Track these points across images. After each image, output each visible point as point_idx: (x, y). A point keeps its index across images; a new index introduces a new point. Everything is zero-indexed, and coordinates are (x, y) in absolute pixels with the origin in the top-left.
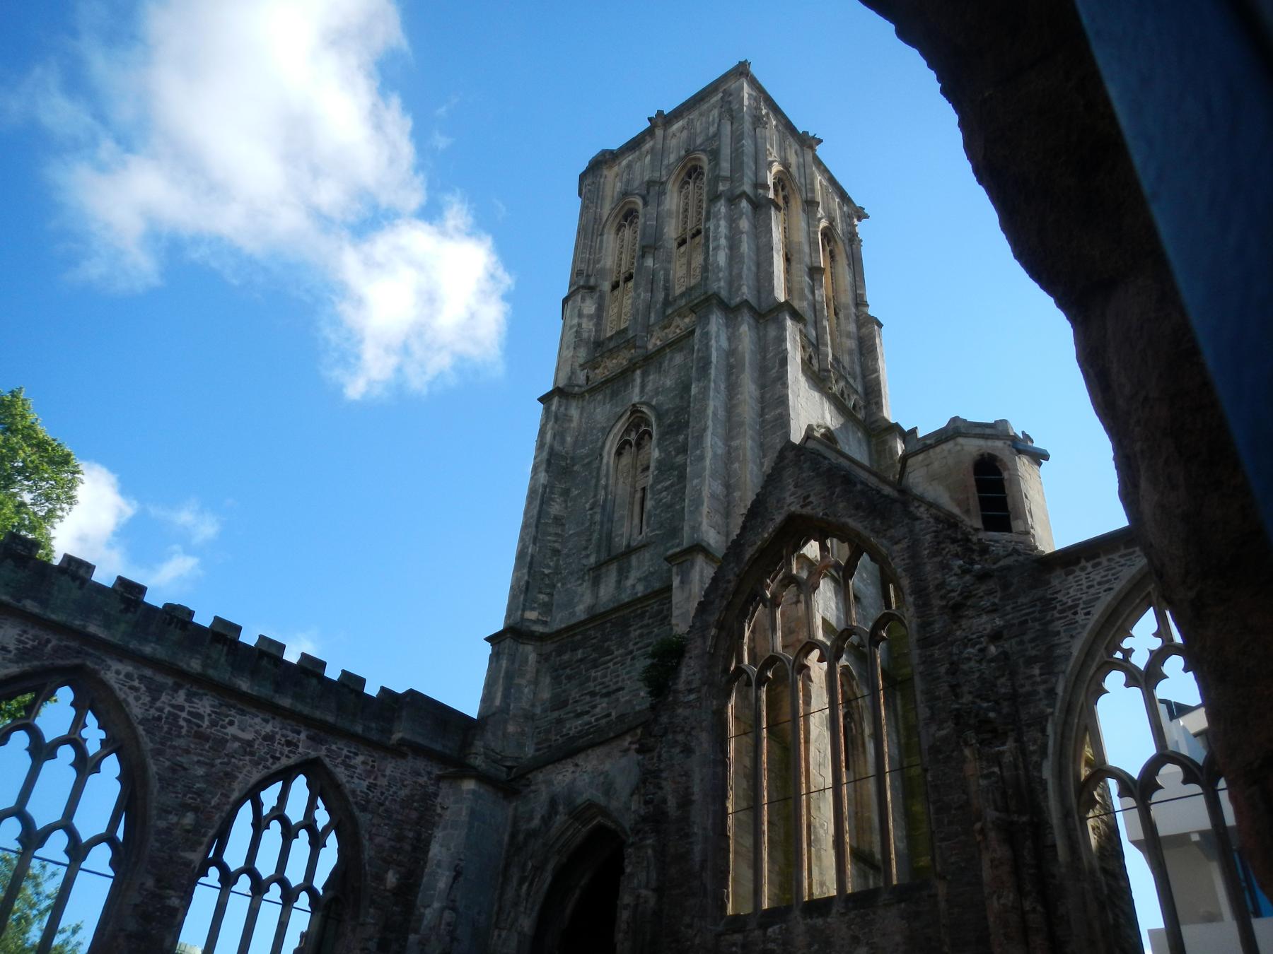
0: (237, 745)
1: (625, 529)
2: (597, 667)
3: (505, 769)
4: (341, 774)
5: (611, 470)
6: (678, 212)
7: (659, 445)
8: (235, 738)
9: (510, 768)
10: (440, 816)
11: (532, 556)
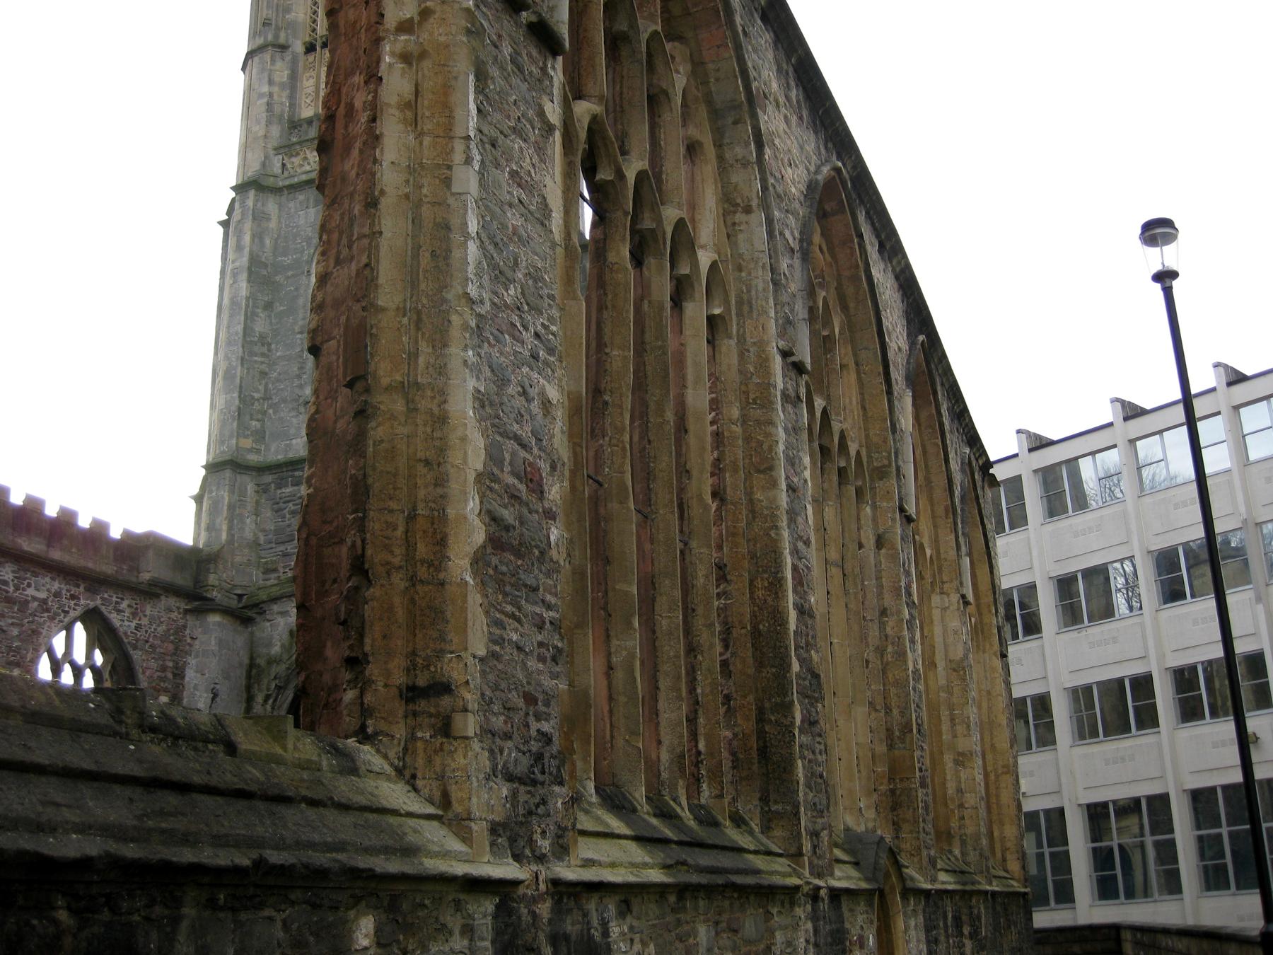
0: (36, 604)
1: (231, 267)
3: (235, 597)
4: (115, 619)
8: (35, 599)
9: (240, 596)
10: (190, 645)
11: (241, 378)
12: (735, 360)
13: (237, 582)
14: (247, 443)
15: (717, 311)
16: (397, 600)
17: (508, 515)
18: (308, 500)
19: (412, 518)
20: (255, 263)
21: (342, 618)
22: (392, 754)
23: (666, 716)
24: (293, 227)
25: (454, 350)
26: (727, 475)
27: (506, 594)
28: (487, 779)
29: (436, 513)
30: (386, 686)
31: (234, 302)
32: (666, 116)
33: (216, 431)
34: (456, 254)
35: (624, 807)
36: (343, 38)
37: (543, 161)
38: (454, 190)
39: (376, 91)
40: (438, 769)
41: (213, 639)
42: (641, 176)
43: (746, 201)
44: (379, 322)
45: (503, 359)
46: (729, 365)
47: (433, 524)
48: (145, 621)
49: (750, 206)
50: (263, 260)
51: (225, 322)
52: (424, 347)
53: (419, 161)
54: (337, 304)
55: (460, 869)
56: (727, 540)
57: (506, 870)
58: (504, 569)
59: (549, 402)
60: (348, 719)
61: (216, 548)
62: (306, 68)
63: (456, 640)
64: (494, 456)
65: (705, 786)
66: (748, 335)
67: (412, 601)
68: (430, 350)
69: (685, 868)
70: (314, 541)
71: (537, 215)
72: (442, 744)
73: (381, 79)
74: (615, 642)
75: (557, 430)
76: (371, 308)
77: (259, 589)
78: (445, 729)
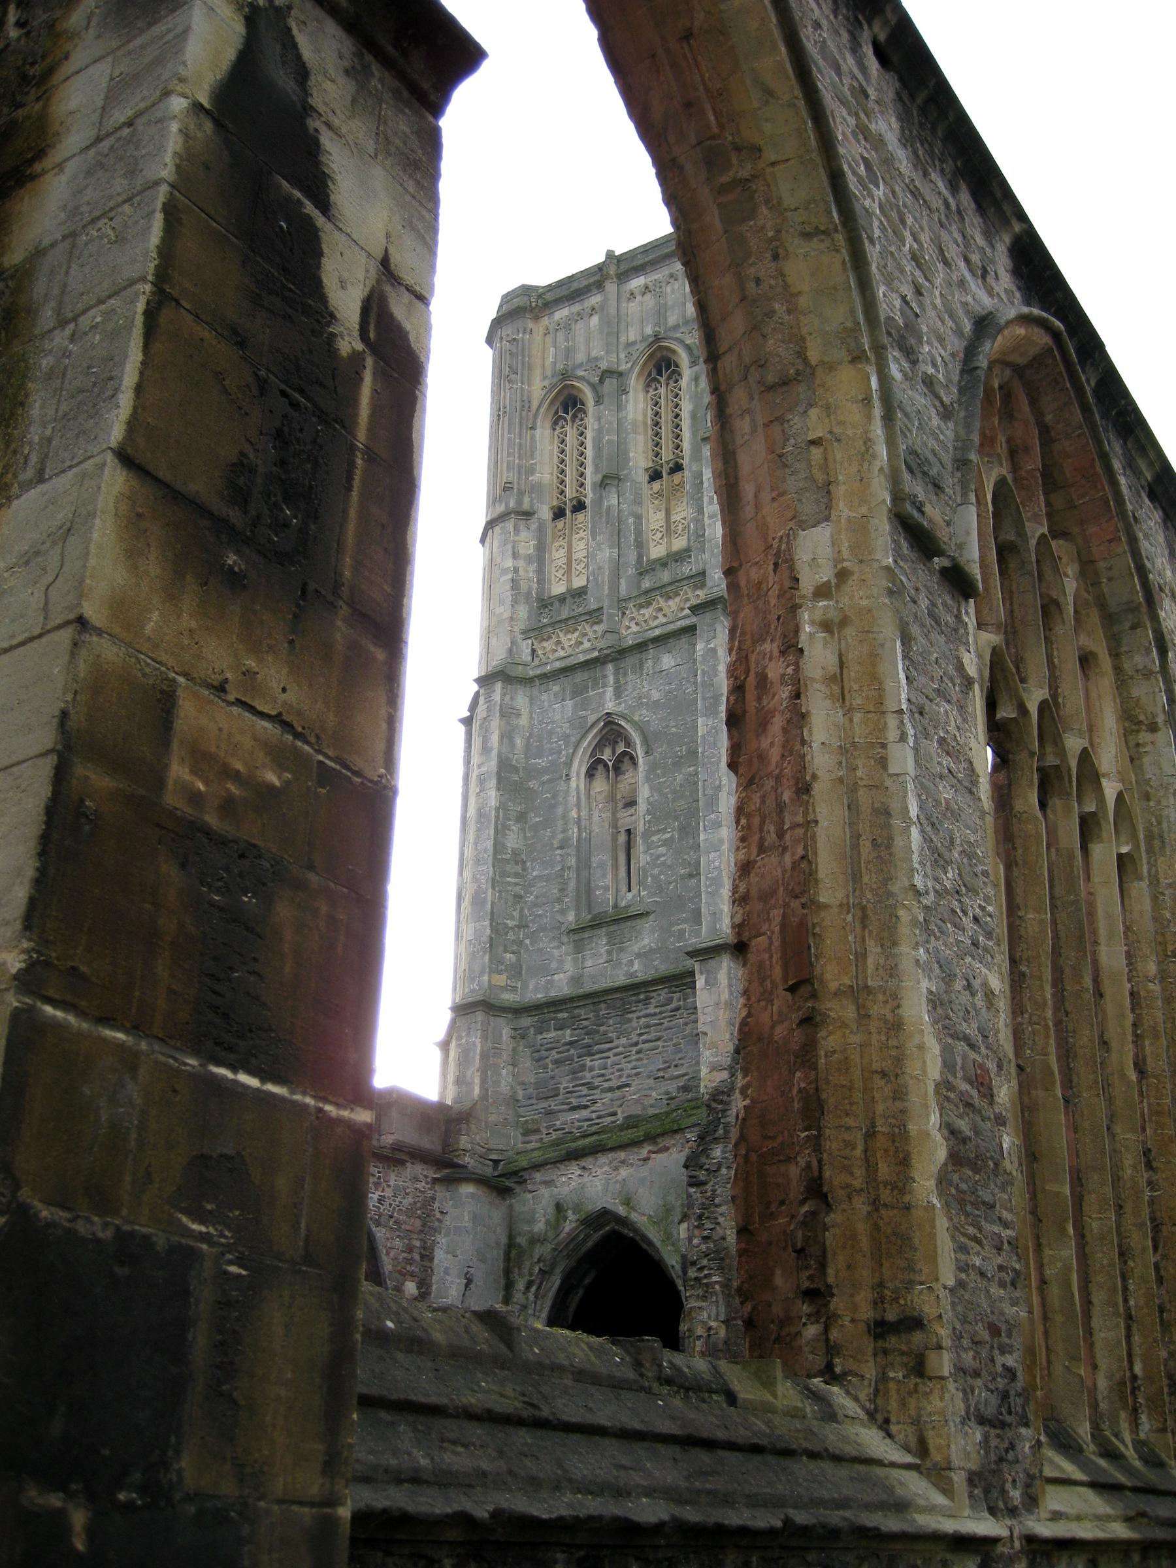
2: (593, 1055)
5: (583, 798)
6: (645, 424)
7: (648, 779)
9: (496, 1162)
10: (440, 1221)
11: (493, 903)
12: (1147, 905)
13: (493, 1145)
14: (501, 980)
15: (1124, 850)
16: (860, 1227)
17: (963, 1125)
18: (746, 1112)
19: (870, 1135)
20: (505, 767)
21: (799, 1246)
22: (862, 1396)
23: (1102, 1335)
24: (548, 724)
25: (904, 949)
26: (1147, 1042)
27: (967, 1215)
28: (963, 1423)
29: (897, 1130)
30: (853, 1321)
31: (481, 815)
32: (1059, 630)
33: (463, 966)
34: (899, 842)
35: (1071, 1447)
36: (746, 600)
37: (965, 720)
38: (891, 771)
39: (797, 665)
40: (913, 1412)
41: (466, 1214)
42: (1043, 706)
43: (1150, 716)
44: (823, 920)
45: (948, 952)
46: (1141, 912)
47: (894, 1141)
48: (388, 1193)
49: (1156, 723)
50: (514, 762)
51: (471, 837)
52: (873, 948)
53: (850, 740)
54: (766, 896)
55: (949, 1526)
56: (1150, 1120)
57: (984, 1526)
58: (964, 1186)
59: (992, 993)
60: (811, 1357)
61: (468, 1105)
62: (555, 537)
63: (926, 1270)
64: (948, 1065)
65: (1144, 1418)
66: (1161, 875)
67: (876, 1227)
68: (879, 950)
69: (1146, 1520)
70: (754, 1157)
71: (966, 784)
72: (916, 1385)
73: (801, 650)
74: (1047, 1252)
75: (1001, 1024)
76: (814, 905)
77: (518, 1153)
78: (919, 1368)
